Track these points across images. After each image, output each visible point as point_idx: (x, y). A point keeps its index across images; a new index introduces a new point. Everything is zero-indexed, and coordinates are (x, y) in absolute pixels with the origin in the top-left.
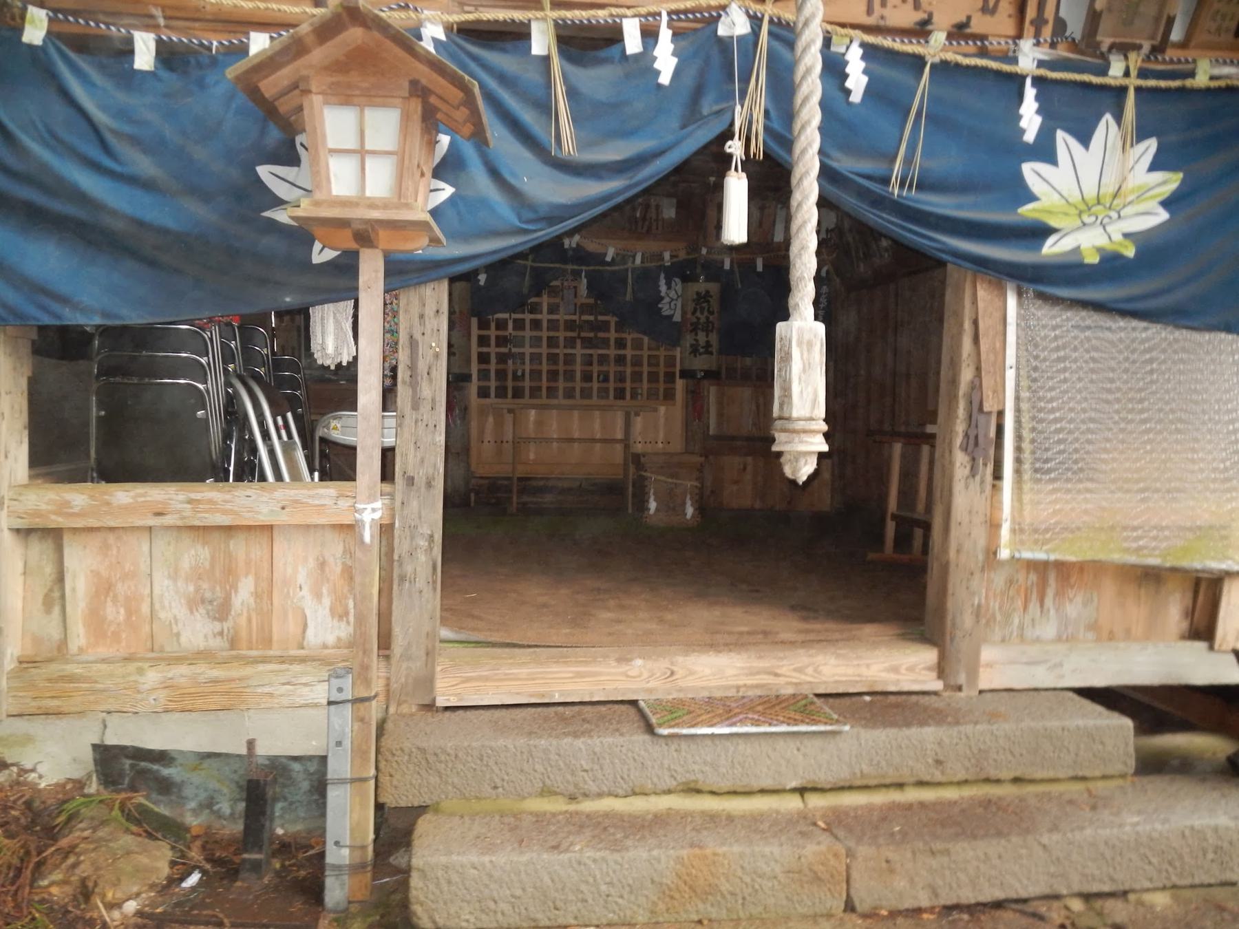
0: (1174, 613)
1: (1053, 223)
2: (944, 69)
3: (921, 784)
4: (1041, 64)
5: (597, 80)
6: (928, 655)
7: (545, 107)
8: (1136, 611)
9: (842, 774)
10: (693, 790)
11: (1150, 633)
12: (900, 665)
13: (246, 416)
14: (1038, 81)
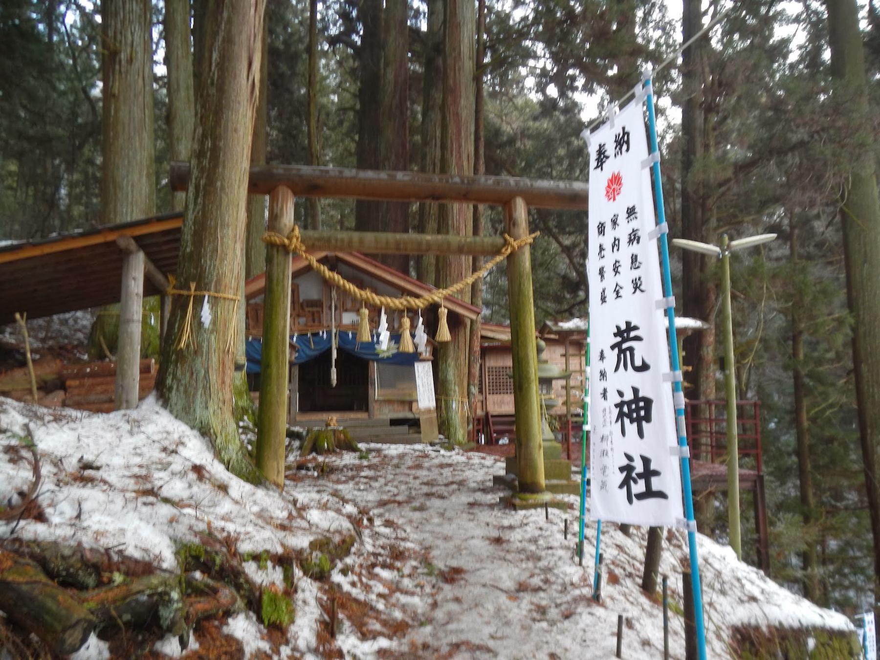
0: (407, 408)
5: (316, 339)
7: (310, 342)
8: (400, 408)
11: (404, 410)
12: (362, 415)
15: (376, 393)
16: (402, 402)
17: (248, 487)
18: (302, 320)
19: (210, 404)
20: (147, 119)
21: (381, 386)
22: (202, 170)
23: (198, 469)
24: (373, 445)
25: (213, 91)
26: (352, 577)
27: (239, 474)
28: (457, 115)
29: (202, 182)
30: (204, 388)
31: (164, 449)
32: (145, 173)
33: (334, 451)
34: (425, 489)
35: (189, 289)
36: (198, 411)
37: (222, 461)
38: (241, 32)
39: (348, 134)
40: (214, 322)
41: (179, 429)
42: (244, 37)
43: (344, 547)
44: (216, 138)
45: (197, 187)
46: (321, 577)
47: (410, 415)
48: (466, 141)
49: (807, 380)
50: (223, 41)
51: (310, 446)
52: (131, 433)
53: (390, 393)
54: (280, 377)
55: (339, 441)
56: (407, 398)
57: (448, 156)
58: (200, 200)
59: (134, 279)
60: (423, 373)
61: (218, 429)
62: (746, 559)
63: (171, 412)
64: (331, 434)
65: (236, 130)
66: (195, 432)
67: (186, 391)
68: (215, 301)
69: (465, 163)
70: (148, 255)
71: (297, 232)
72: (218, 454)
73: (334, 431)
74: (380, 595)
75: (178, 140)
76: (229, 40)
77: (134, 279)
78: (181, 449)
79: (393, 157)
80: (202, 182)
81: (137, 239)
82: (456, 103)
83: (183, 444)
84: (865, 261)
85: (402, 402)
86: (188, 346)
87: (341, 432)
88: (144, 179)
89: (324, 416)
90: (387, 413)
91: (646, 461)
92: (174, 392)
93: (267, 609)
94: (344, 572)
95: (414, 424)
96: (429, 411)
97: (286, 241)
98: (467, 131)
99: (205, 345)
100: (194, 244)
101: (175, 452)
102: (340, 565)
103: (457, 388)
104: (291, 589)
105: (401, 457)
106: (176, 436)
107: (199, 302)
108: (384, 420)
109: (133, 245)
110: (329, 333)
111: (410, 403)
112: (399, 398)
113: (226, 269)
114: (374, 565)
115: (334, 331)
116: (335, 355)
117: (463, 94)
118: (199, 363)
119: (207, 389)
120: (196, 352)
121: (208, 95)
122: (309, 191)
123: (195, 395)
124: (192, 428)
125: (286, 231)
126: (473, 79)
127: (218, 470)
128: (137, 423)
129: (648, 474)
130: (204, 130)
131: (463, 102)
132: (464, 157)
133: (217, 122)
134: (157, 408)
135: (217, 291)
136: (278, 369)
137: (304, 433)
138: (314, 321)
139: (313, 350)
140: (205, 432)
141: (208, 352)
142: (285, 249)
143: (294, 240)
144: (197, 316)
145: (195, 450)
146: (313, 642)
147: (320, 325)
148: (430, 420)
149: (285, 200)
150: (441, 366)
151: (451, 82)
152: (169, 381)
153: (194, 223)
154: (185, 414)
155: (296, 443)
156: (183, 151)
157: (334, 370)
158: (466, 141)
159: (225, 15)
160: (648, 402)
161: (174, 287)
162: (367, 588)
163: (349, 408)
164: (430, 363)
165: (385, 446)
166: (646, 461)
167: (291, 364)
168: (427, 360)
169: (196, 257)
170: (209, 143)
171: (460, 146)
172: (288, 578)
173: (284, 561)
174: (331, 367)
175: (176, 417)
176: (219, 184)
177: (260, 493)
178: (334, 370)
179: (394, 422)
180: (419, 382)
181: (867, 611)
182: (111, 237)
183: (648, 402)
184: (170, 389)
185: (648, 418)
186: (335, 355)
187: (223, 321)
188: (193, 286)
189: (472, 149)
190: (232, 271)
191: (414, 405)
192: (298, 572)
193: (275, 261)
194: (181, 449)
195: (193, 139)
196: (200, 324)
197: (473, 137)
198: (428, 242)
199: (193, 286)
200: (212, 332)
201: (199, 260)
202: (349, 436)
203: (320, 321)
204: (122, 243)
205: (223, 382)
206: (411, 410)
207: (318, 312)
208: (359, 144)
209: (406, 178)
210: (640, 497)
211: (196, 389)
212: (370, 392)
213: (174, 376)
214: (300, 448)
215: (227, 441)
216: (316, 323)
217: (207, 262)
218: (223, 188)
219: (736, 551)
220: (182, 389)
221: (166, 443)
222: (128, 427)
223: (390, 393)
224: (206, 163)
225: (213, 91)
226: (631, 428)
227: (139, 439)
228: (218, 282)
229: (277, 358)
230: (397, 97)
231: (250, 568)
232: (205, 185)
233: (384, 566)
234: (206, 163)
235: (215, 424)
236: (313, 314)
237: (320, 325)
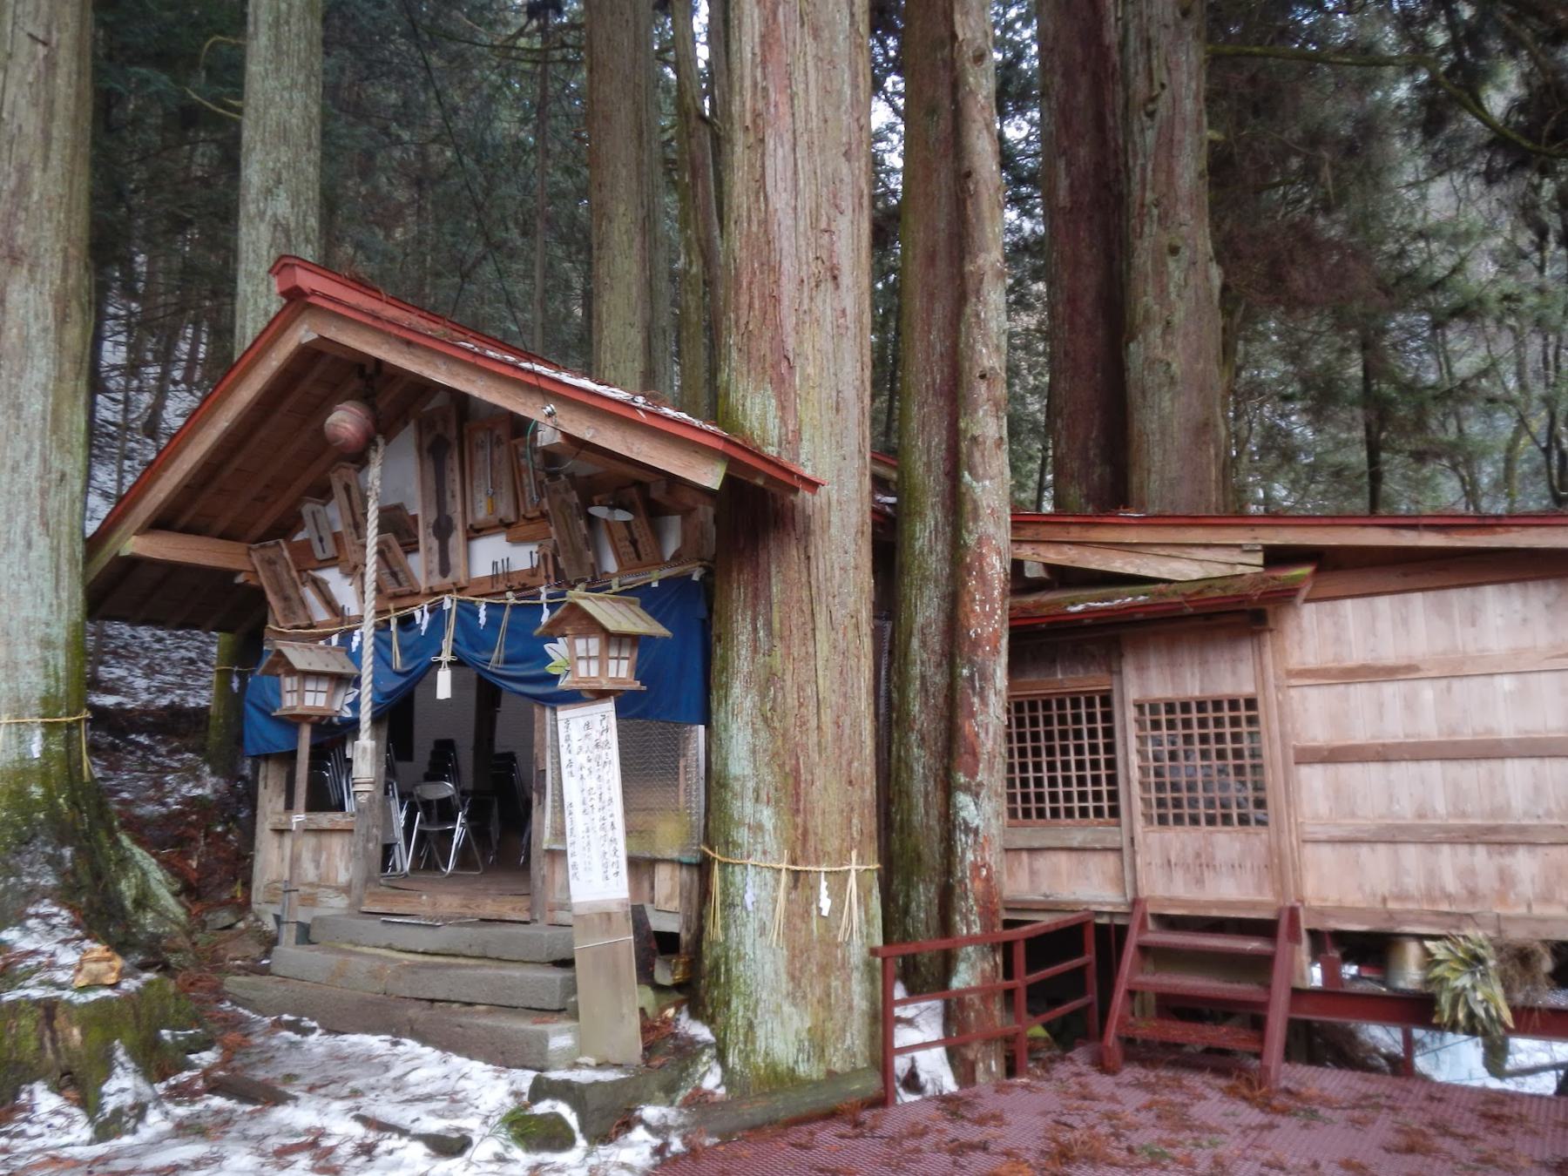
1: (554, 672)
2: (514, 607)
3: (465, 956)
4: (549, 596)
6: (522, 903)
9: (433, 948)
10: (389, 947)
13: (544, 787)
14: (549, 605)
103: (767, 816)
164: (609, 707)
168: (601, 695)
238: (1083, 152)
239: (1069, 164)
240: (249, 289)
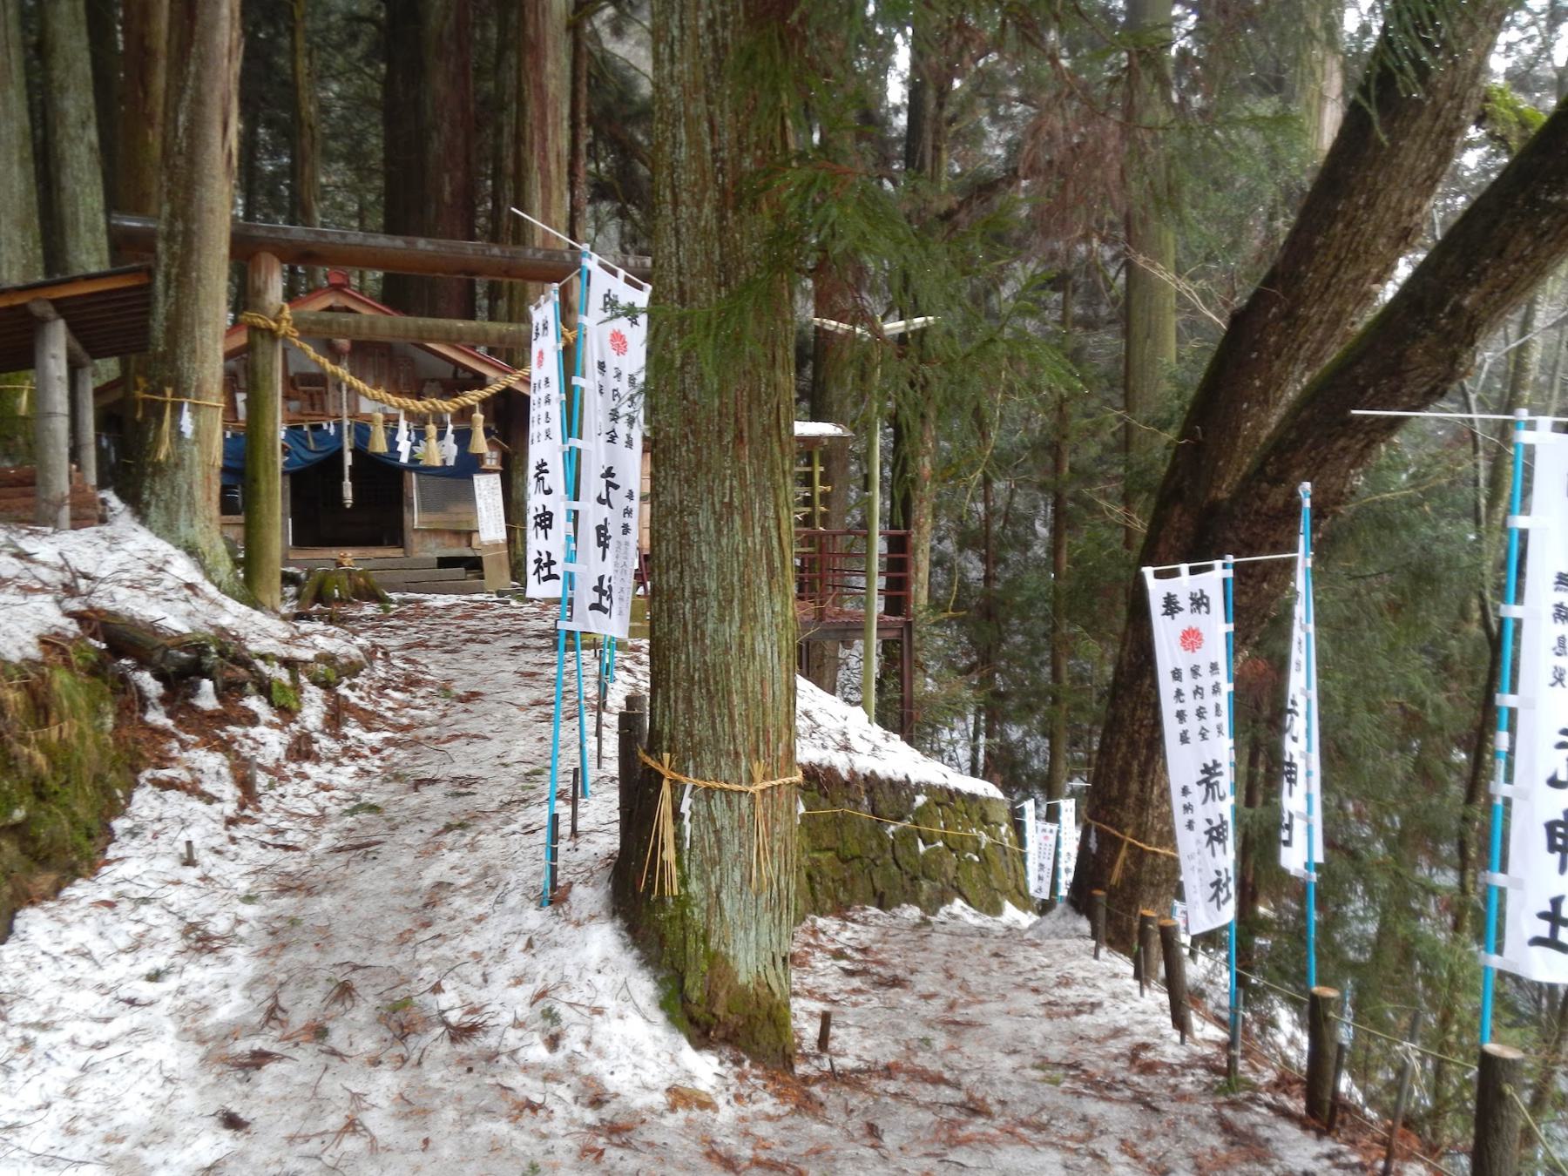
0: (464, 542)
5: (318, 434)
7: (306, 439)
8: (454, 541)
11: (459, 545)
15: (416, 518)
16: (456, 533)
17: (244, 609)
18: (294, 405)
19: (196, 522)
20: (13, 66)
21: (424, 508)
22: (173, 256)
23: (190, 586)
24: (410, 595)
25: (181, 161)
26: (358, 693)
27: (232, 595)
28: (540, 87)
29: (174, 271)
30: (189, 504)
31: (151, 567)
32: (16, 157)
33: (350, 602)
34: (467, 636)
35: (164, 395)
36: (182, 529)
37: (212, 582)
38: (212, 91)
39: (368, 58)
40: (196, 432)
41: (162, 548)
42: (217, 94)
43: (353, 669)
44: (188, 220)
45: (167, 275)
46: (327, 686)
47: (469, 553)
48: (555, 132)
49: (1070, 505)
50: (192, 100)
51: (313, 594)
52: (109, 549)
53: (437, 519)
54: (270, 494)
55: (357, 586)
56: (465, 528)
57: (526, 154)
58: (171, 292)
59: (54, 357)
60: (487, 490)
61: (206, 549)
62: (882, 721)
63: (151, 529)
64: (344, 577)
65: (212, 211)
66: (181, 552)
67: (167, 508)
68: (196, 409)
69: (553, 168)
70: (73, 328)
71: (287, 313)
72: (208, 574)
73: (349, 572)
74: (390, 709)
75: (63, 89)
76: (199, 101)
77: (54, 357)
78: (167, 567)
79: (446, 126)
80: (174, 271)
81: (54, 302)
82: (538, 67)
83: (168, 562)
84: (1148, 336)
85: (456, 533)
86: (168, 457)
87: (360, 574)
88: (16, 169)
89: (335, 553)
90: (434, 549)
91: (549, 554)
92: (152, 508)
93: (276, 694)
94: (352, 687)
95: (474, 565)
96: (496, 546)
97: (273, 325)
98: (555, 116)
99: (187, 457)
100: (167, 343)
101: (161, 570)
102: (346, 682)
104: (297, 688)
105: (448, 608)
106: (159, 555)
107: (177, 409)
108: (426, 560)
109: (50, 311)
110: (339, 426)
111: (469, 534)
112: (453, 527)
113: (207, 372)
114: (384, 687)
115: (346, 423)
116: (348, 460)
117: (550, 52)
118: (181, 477)
119: (191, 505)
120: (177, 465)
121: (176, 166)
122: (300, 259)
123: (177, 512)
124: (177, 547)
125: (273, 311)
126: (568, 28)
127: (211, 590)
128: (114, 540)
129: (551, 563)
130: (173, 209)
131: (550, 67)
132: (552, 156)
133: (189, 200)
134: (135, 526)
135: (198, 398)
136: (268, 483)
137: (303, 576)
138: (313, 406)
139: (312, 452)
140: (191, 551)
141: (191, 466)
142: (272, 335)
143: (284, 324)
144: (176, 425)
145: (182, 568)
146: (320, 727)
147: (324, 414)
148: (497, 559)
149: (269, 271)
150: (516, 480)
151: (531, 31)
152: (146, 496)
153: (167, 319)
154: (167, 531)
155: (292, 590)
156: (72, 110)
157: (347, 485)
158: (555, 132)
159: (192, 68)
160: (551, 514)
161: (146, 391)
162: (377, 703)
163: (376, 542)
164: (497, 476)
165: (428, 597)
166: (549, 554)
167: (284, 473)
168: (495, 471)
169: (170, 359)
170: (179, 226)
171: (545, 139)
172: (294, 678)
173: (288, 663)
174: (342, 479)
175: (157, 535)
176: (194, 274)
177: (258, 615)
178: (347, 485)
179: (444, 562)
180: (480, 503)
181: (1069, 797)
182: (19, 300)
183: (551, 514)
184: (148, 505)
185: (550, 526)
186: (348, 460)
187: (198, 431)
188: (169, 391)
189: (564, 144)
190: (213, 375)
191: (475, 536)
192: (304, 679)
193: (259, 350)
194: (167, 567)
195: (469, 794)
196: (180, 434)
197: (566, 124)
198: (459, 329)
199: (169, 391)
200: (194, 443)
201: (174, 361)
202: (374, 580)
203: (323, 408)
204: (37, 309)
205: (209, 499)
206: (470, 545)
207: (319, 393)
208: (388, 83)
209: (430, 247)
210: (545, 579)
211: (179, 505)
212: (407, 516)
213: (152, 492)
214: (297, 597)
215: (216, 563)
216: (318, 412)
217: (185, 364)
218: (199, 279)
219: (867, 712)
220: (162, 504)
221: (152, 561)
222: (106, 544)
223: (437, 519)
224: (177, 248)
225: (181, 161)
226: (541, 533)
227: (120, 557)
228: (199, 388)
229: (266, 471)
230: (452, 17)
231: (260, 663)
232: (178, 275)
233: (396, 689)
234: (177, 248)
235: (203, 545)
236: (311, 396)
237: (324, 414)
238: (459, 174)
239: (451, 179)
240: (78, 189)
